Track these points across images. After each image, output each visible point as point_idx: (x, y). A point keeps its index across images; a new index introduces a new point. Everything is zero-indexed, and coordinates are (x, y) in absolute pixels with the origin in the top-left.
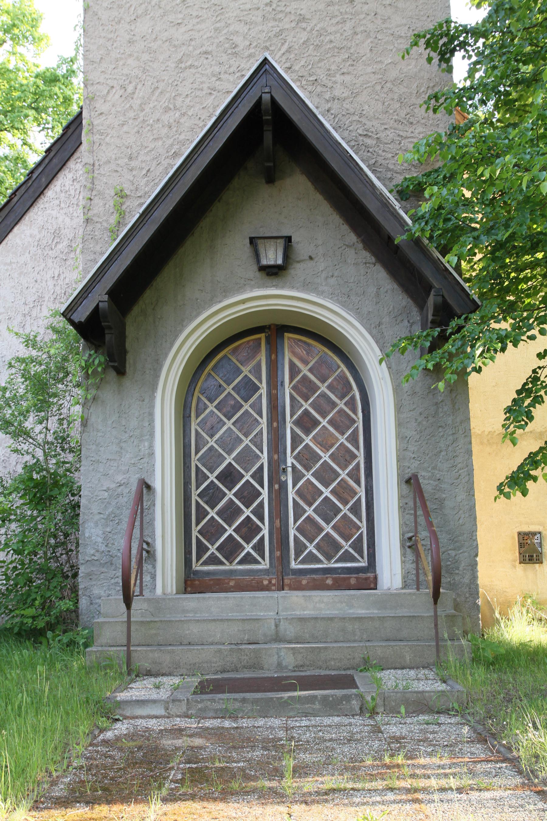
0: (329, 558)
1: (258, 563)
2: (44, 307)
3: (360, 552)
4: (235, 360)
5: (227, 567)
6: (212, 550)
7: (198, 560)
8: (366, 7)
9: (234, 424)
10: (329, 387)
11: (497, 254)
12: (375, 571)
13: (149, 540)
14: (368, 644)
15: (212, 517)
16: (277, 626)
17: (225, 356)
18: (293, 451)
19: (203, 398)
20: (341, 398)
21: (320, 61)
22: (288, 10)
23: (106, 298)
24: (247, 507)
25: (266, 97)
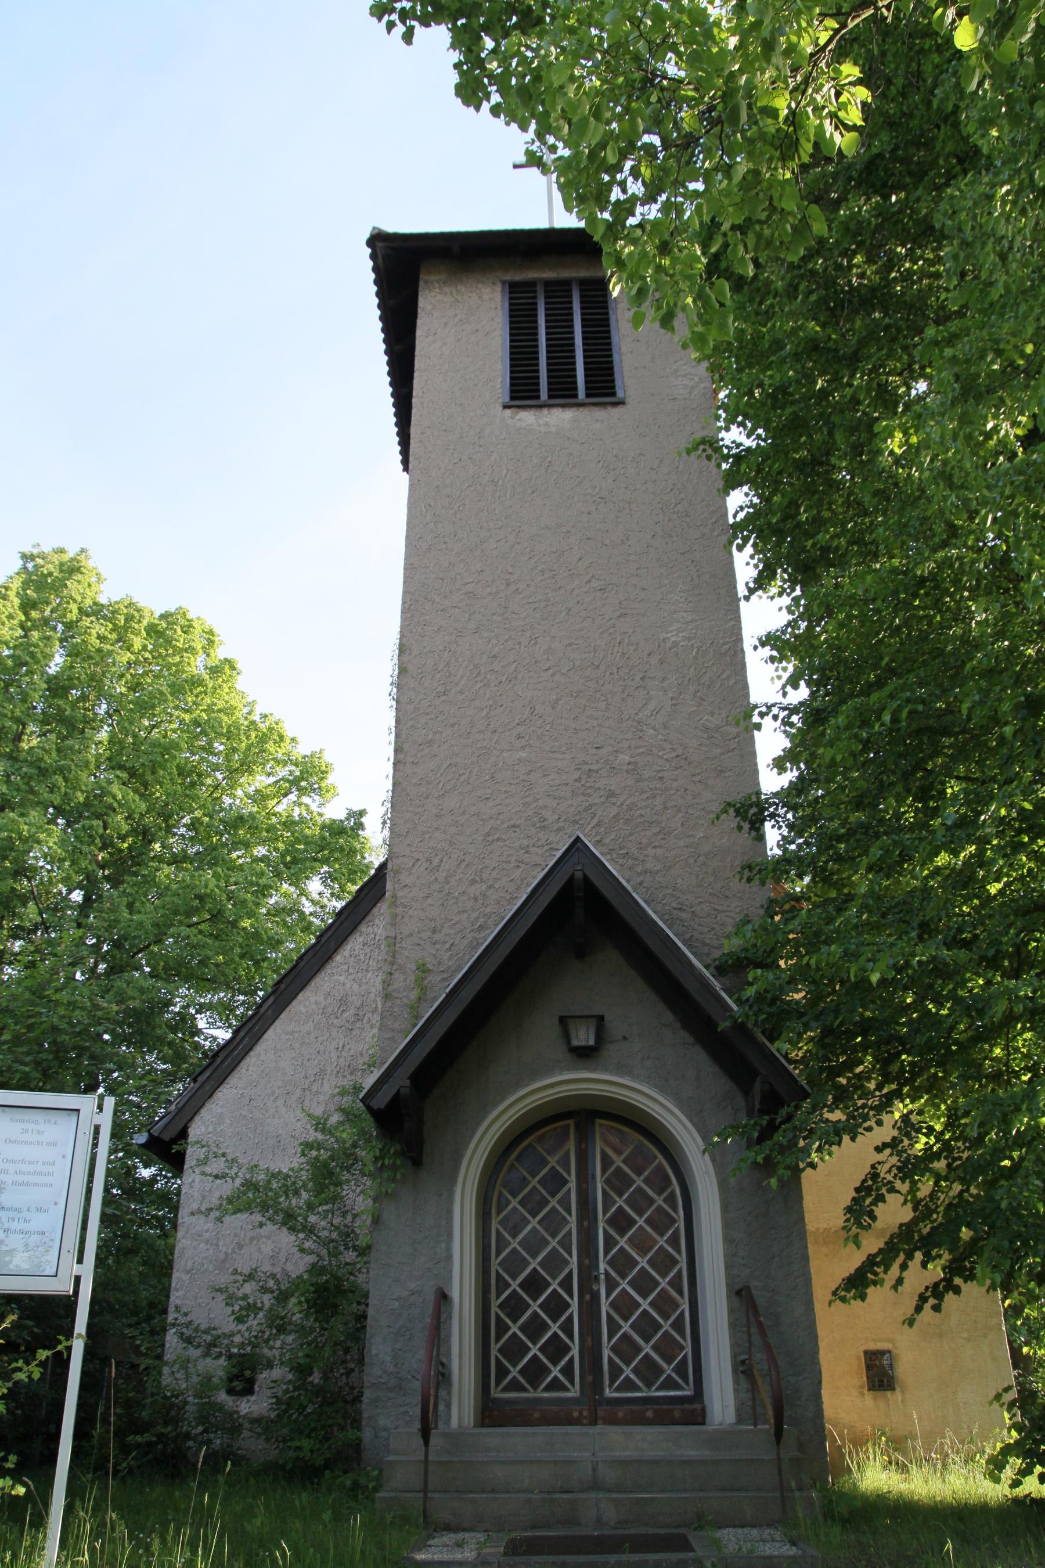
0: (649, 1385)
1: (567, 1389)
2: (325, 1082)
3: (685, 1379)
4: (540, 1150)
5: (531, 1394)
6: (514, 1372)
7: (497, 1384)
8: (675, 784)
9: (539, 1223)
10: (646, 1181)
11: (826, 1041)
12: (702, 1402)
13: (444, 1360)
14: (701, 1494)
15: (514, 1333)
16: (594, 1470)
17: (530, 1145)
18: (606, 1254)
19: (505, 1192)
20: (659, 1194)
21: (631, 834)
22: (597, 785)
23: (408, 1083)
24: (555, 1322)
25: (579, 875)
